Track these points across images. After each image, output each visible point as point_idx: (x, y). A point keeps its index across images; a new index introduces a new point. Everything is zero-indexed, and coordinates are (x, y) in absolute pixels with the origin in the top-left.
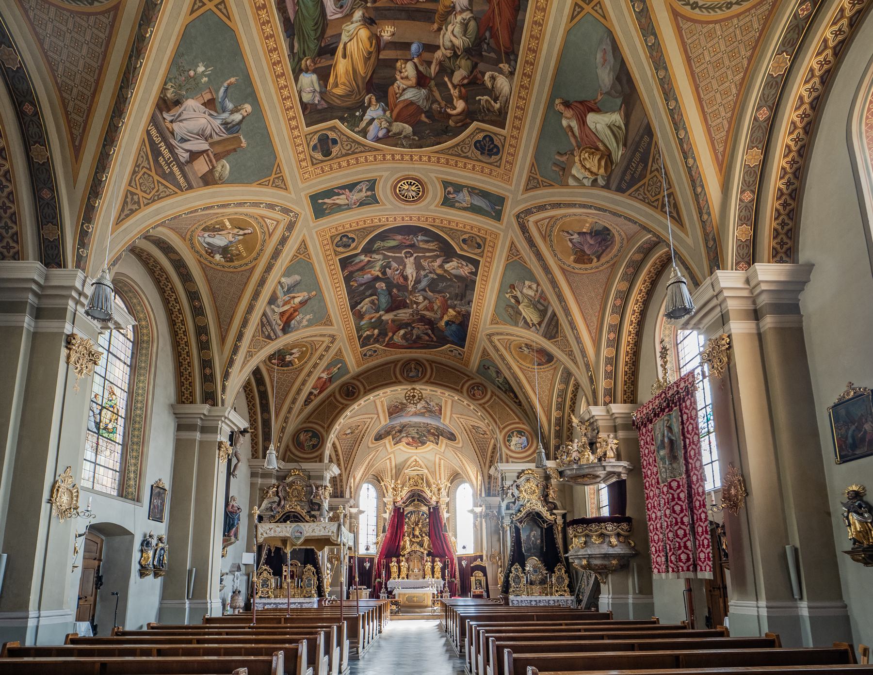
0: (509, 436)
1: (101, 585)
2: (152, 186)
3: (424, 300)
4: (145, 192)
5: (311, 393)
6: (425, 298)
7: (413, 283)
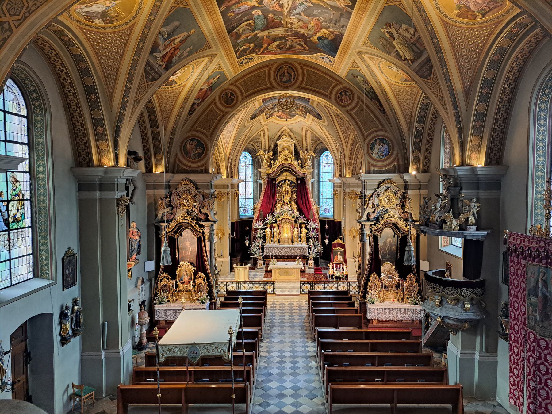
0: (371, 149)
1: (30, 360)
2: (21, 5)
3: (299, 21)
4: (14, 15)
5: (194, 104)
6: (299, 20)
7: (288, 9)
